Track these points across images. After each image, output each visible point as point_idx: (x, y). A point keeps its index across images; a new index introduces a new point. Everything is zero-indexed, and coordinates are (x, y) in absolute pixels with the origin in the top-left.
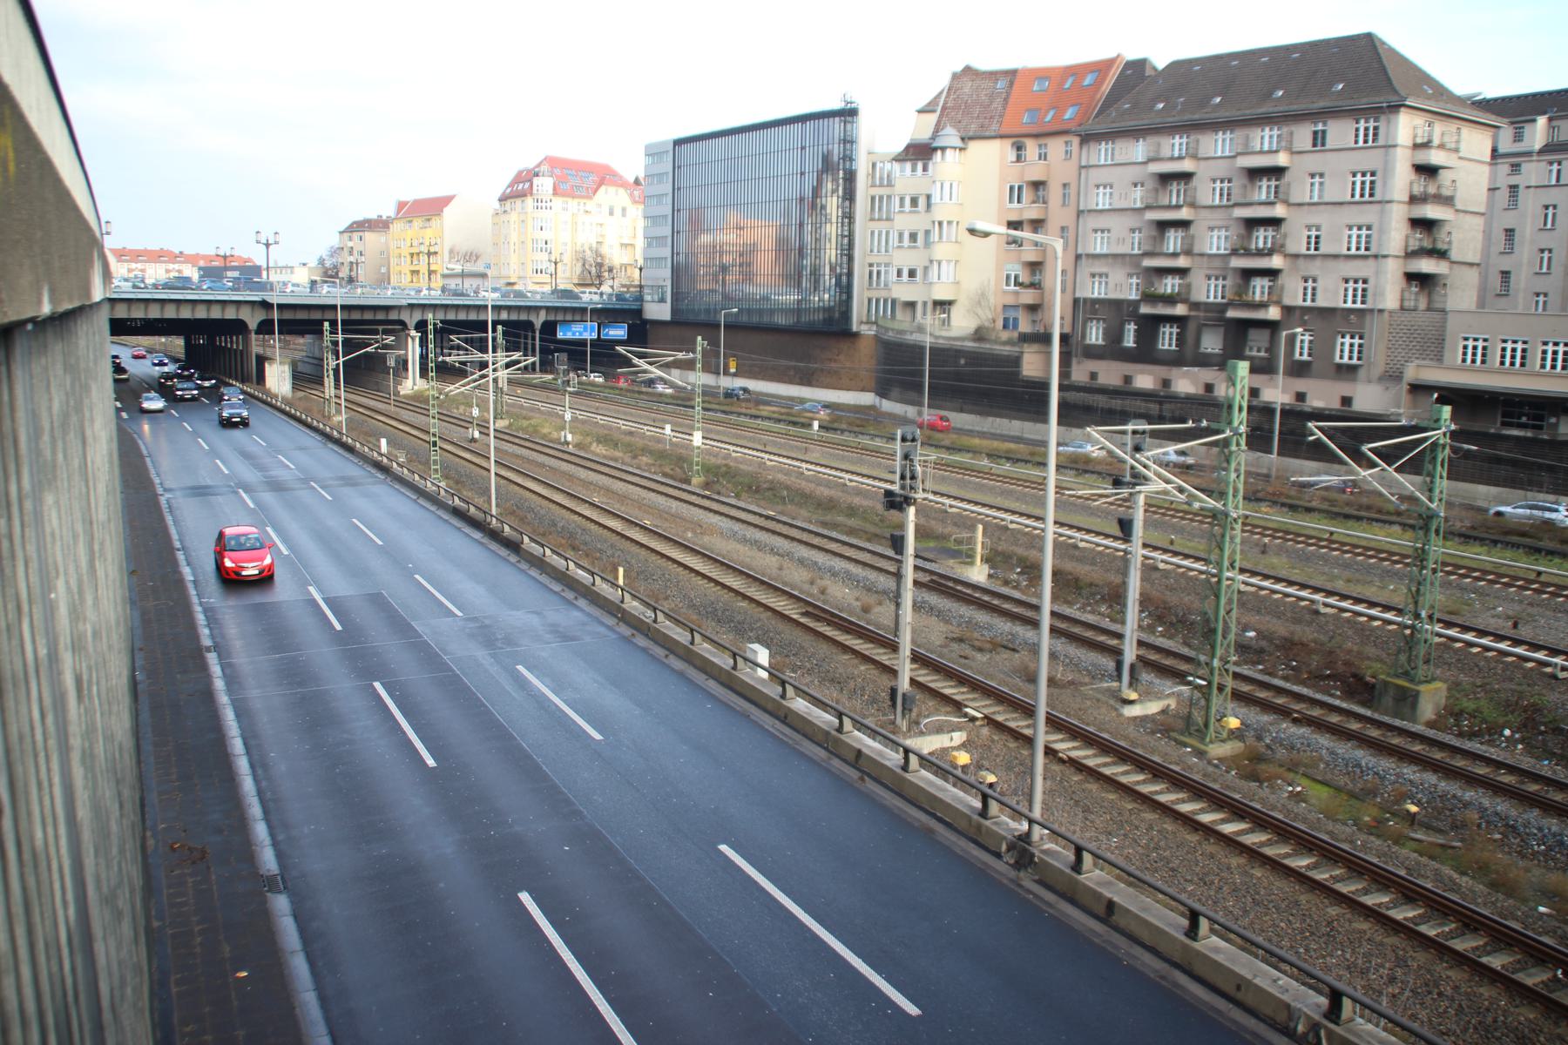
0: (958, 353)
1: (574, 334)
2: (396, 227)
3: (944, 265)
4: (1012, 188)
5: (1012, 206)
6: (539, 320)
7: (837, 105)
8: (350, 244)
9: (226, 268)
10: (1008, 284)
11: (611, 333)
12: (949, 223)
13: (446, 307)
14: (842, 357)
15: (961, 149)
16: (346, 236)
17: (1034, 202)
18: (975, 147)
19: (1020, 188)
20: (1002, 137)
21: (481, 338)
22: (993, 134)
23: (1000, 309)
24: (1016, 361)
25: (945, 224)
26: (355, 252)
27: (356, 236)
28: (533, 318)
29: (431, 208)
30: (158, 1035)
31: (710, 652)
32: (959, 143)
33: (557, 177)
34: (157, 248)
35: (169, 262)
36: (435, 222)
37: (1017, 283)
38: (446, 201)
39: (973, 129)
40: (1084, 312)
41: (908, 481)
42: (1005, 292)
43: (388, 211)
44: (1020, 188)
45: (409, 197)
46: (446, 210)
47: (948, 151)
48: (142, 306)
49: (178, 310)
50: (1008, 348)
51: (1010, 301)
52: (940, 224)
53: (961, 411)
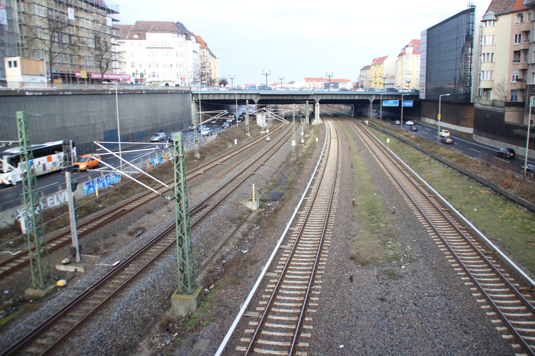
0: (487, 111)
1: (389, 105)
2: (372, 68)
3: (485, 72)
4: (516, 35)
5: (516, 44)
6: (372, 99)
7: (466, 8)
8: (363, 74)
9: (330, 83)
10: (513, 80)
11: (407, 104)
12: (488, 54)
13: (323, 95)
14: (468, 114)
15: (494, 21)
16: (362, 71)
17: (525, 41)
18: (501, 19)
19: (520, 35)
20: (512, 12)
22: (508, 12)
23: (509, 91)
24: (502, 115)
25: (486, 55)
26: (364, 77)
27: (364, 71)
28: (369, 98)
29: (380, 61)
31: (73, 222)
32: (494, 18)
33: (415, 47)
34: (342, 78)
35: (310, 81)
36: (382, 65)
37: (517, 80)
38: (385, 58)
39: (501, 10)
40: (529, 91)
41: (68, 161)
42: (512, 84)
43: (370, 63)
44: (520, 35)
45: (377, 57)
46: (385, 61)
47: (488, 22)
48: (218, 95)
49: (213, 97)
50: (500, 109)
51: (514, 88)
52: (484, 54)
53: (487, 137)
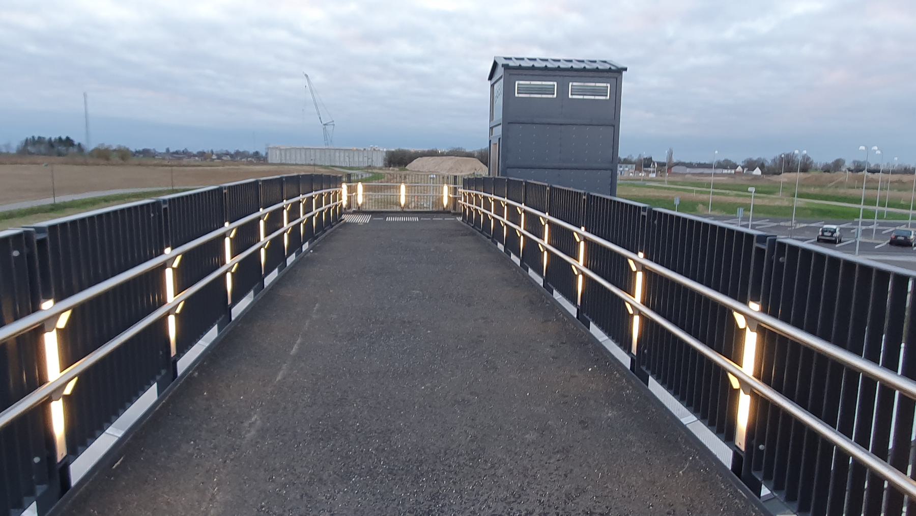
21: (682, 220)
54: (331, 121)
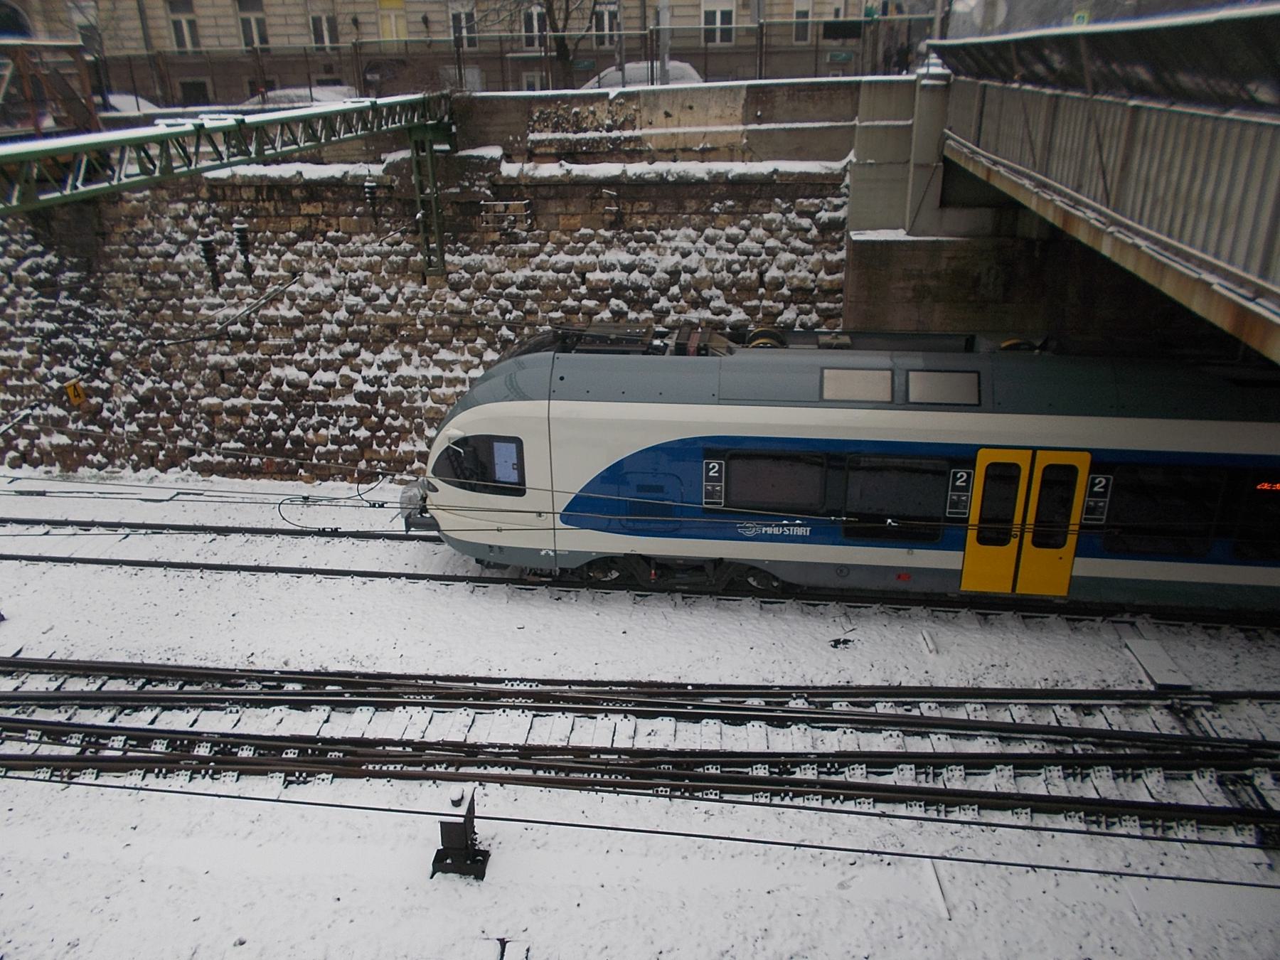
30: (1057, 601)
54: (49, 627)
